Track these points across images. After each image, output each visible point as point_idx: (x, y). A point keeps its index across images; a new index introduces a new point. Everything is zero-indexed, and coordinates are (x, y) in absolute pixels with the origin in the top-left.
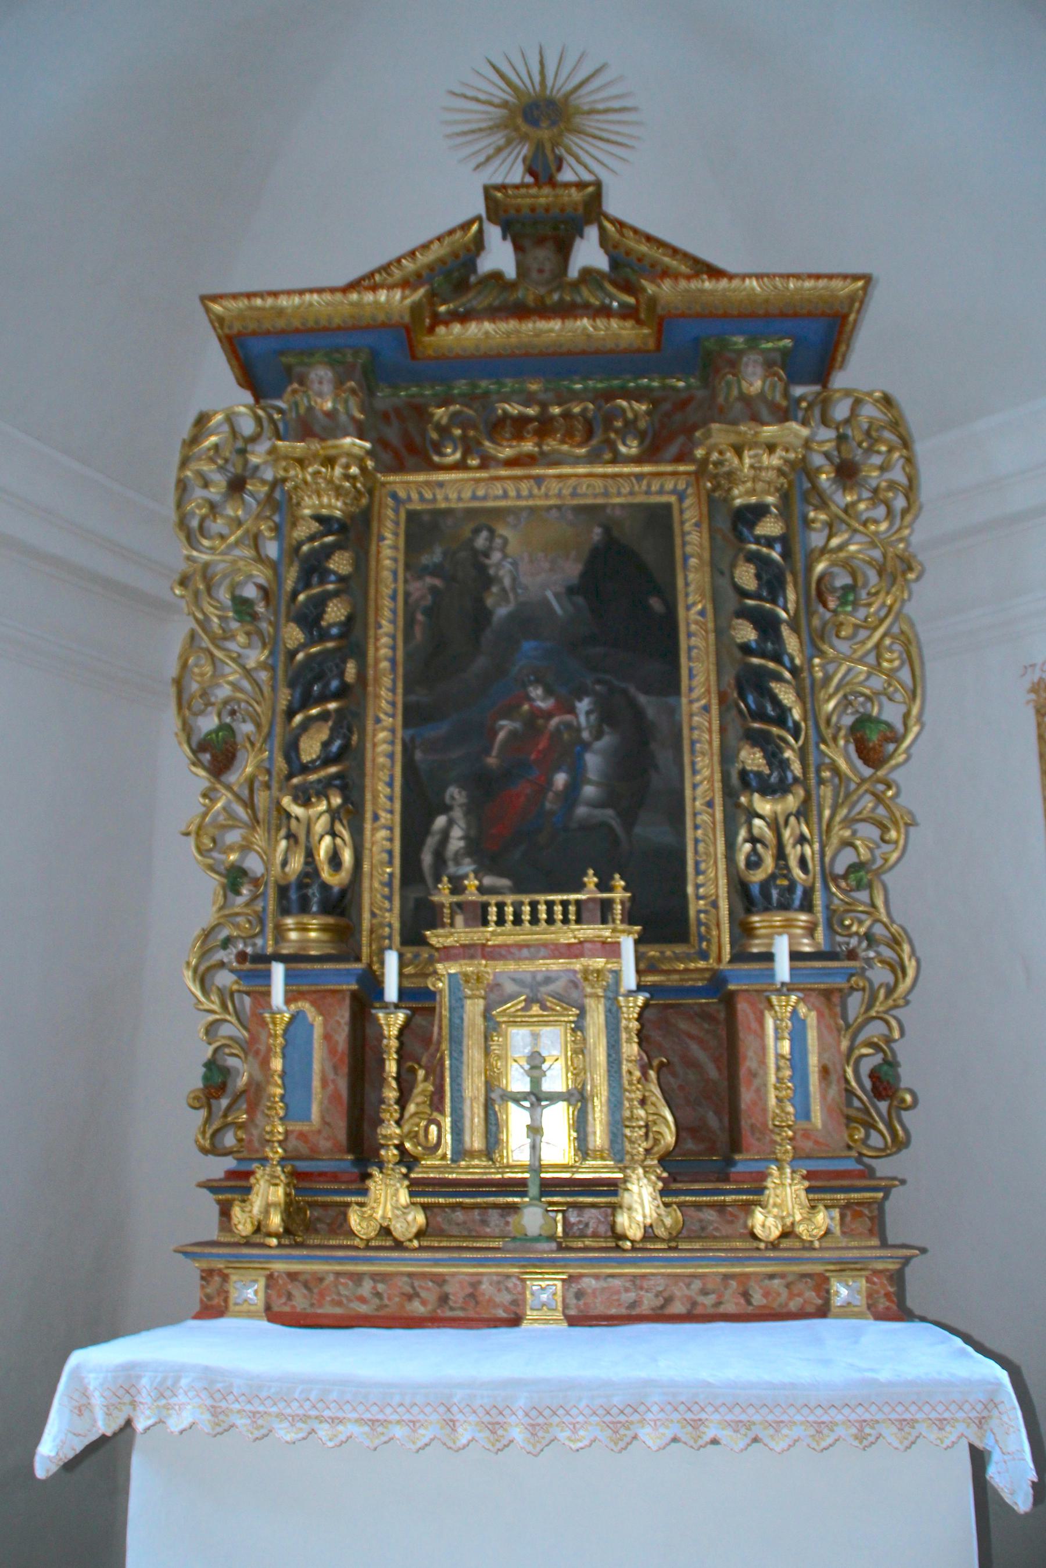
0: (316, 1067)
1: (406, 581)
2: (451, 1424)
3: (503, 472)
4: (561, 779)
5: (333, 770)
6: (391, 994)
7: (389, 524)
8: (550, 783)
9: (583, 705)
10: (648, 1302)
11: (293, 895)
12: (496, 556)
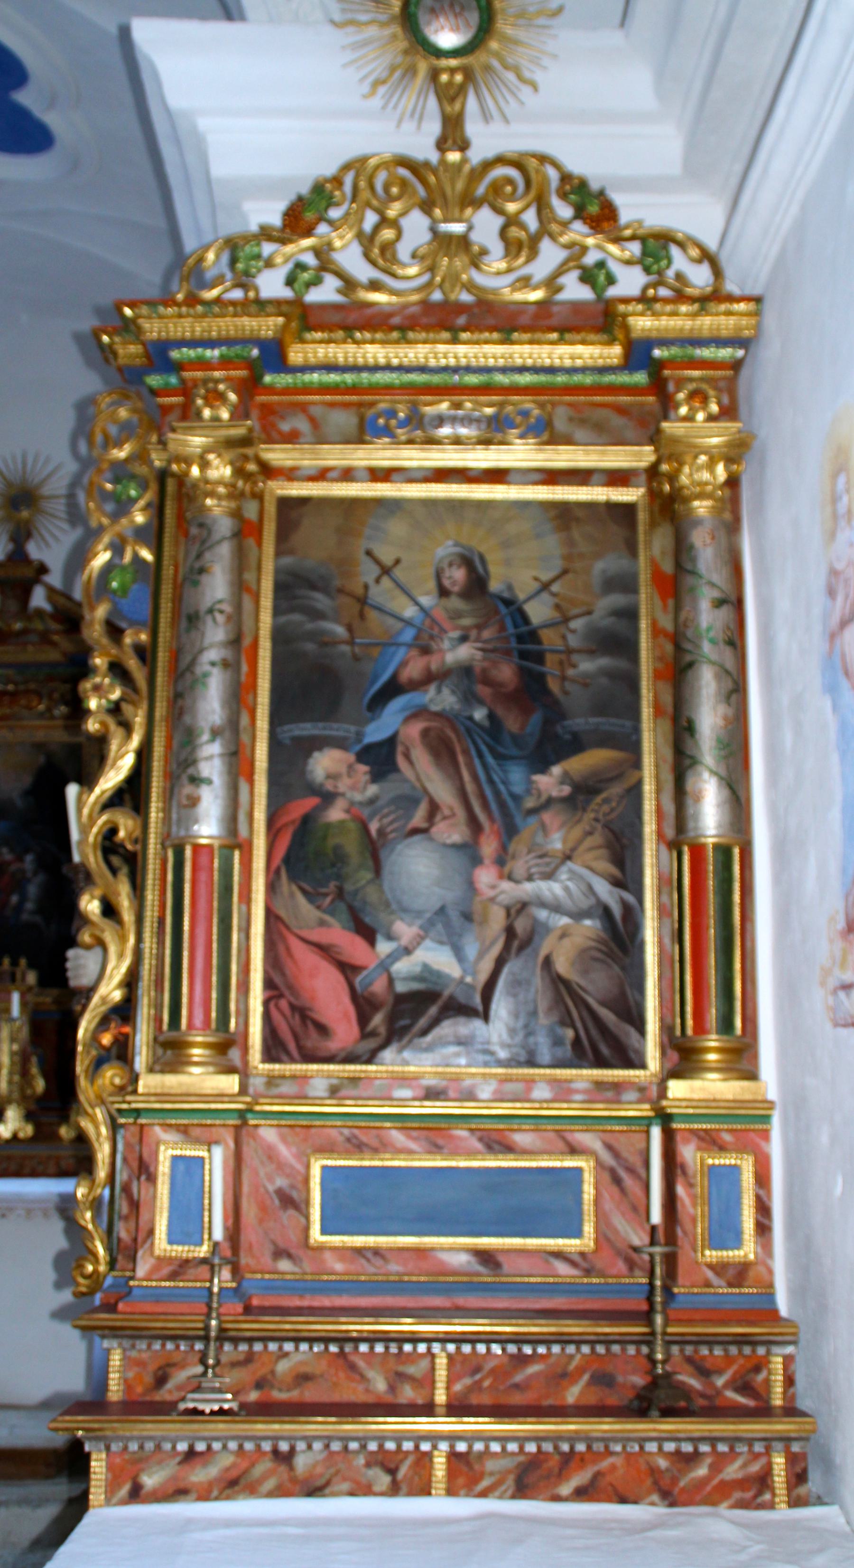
4: (14, 899)
9: (29, 858)
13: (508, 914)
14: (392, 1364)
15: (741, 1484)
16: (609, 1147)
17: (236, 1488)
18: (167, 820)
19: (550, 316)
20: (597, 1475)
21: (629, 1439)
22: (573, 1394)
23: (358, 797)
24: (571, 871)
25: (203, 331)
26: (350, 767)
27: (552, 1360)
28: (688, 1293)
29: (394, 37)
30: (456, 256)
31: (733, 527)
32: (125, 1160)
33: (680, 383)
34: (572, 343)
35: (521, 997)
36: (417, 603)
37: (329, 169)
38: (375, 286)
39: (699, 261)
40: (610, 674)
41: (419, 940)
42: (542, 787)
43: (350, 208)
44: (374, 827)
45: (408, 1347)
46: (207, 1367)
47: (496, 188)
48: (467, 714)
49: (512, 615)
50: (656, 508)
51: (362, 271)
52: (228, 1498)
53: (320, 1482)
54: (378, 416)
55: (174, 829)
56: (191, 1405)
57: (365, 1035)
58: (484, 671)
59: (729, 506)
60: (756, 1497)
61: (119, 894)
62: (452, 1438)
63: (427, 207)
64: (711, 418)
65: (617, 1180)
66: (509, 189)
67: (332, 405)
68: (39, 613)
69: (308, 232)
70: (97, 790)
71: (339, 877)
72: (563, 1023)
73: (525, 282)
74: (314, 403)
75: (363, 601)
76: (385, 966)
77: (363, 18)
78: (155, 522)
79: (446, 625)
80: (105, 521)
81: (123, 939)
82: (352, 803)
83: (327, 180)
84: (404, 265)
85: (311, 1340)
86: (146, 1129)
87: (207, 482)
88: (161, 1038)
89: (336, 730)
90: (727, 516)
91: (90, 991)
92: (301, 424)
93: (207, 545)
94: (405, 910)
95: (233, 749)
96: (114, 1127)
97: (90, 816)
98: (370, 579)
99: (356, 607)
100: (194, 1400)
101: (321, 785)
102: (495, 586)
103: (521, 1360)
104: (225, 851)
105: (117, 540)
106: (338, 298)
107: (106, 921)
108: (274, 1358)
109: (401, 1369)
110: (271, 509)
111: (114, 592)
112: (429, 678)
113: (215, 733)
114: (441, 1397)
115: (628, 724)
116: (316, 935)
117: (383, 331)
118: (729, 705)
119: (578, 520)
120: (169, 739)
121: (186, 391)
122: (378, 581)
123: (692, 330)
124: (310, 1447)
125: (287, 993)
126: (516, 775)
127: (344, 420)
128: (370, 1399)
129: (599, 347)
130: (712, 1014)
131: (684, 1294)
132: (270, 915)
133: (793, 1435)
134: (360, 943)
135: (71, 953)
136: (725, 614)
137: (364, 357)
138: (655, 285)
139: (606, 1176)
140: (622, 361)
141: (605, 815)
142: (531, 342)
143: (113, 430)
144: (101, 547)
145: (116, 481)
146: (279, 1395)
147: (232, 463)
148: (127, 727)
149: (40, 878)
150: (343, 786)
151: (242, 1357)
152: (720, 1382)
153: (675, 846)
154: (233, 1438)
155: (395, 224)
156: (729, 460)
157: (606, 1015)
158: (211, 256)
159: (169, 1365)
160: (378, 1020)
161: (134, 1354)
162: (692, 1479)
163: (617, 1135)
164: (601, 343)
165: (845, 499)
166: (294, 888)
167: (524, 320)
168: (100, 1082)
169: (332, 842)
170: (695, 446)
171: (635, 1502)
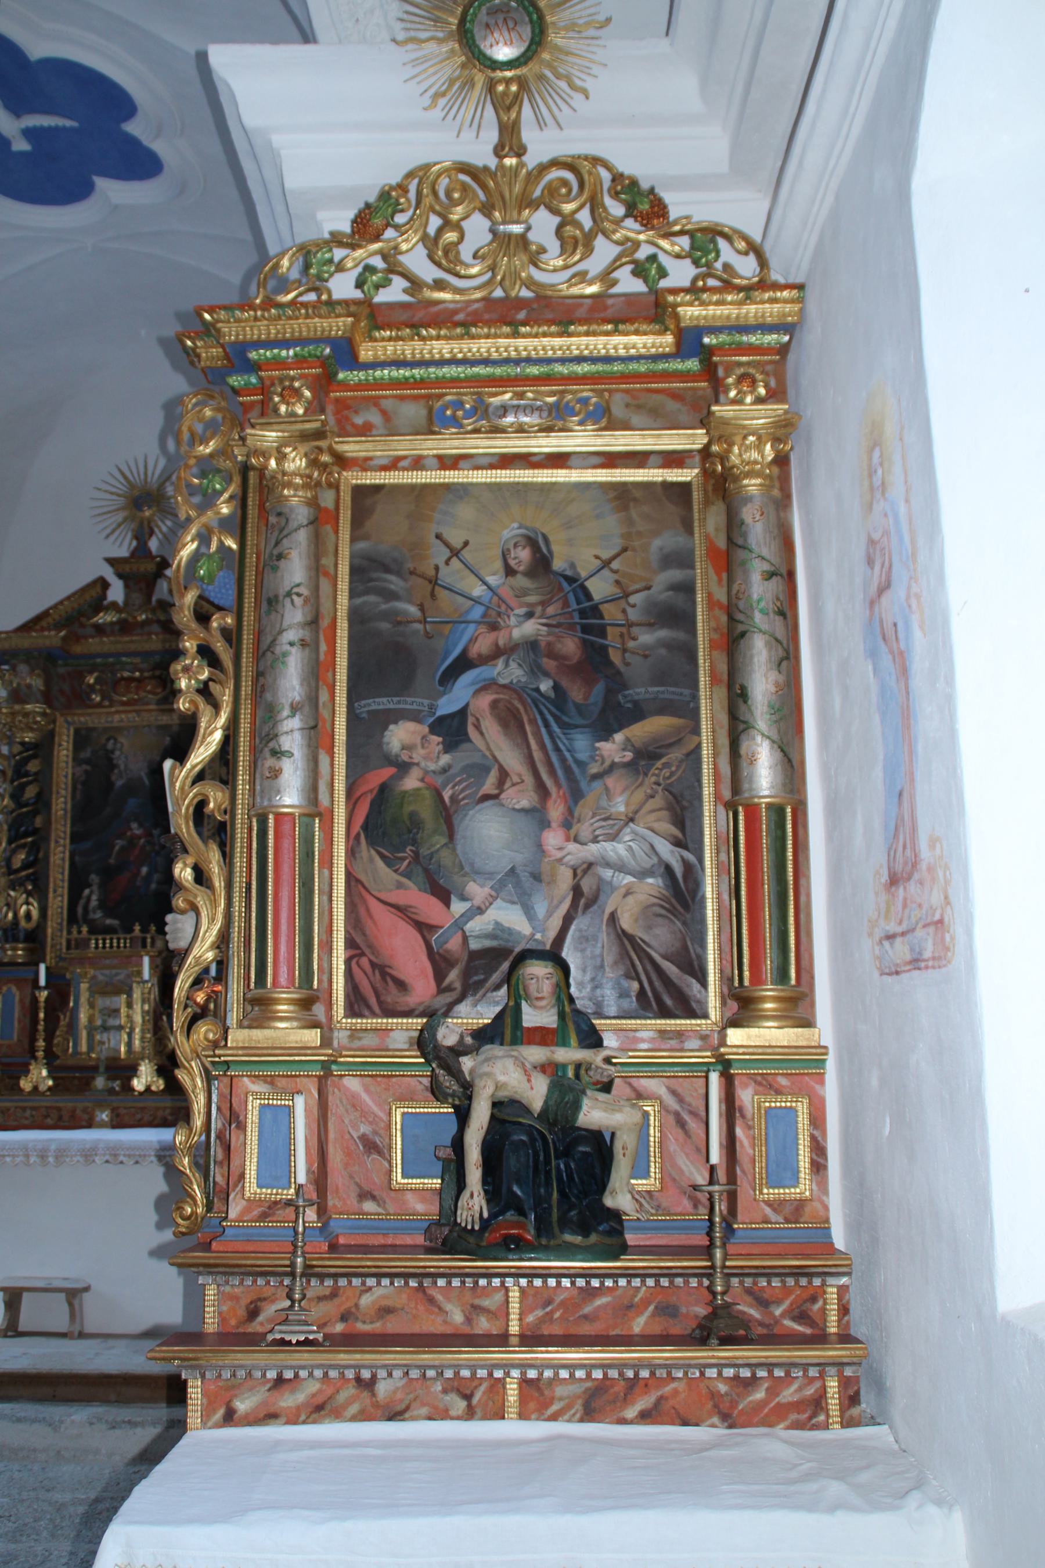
0: (16, 1015)
1: (73, 767)
2: (27, 1156)
3: (121, 708)
4: (144, 870)
5: (31, 871)
6: (42, 982)
7: (65, 738)
8: (139, 871)
11: (10, 933)
12: (117, 753)
13: (575, 875)
14: (468, 1296)
15: (796, 1406)
16: (673, 1092)
17: (322, 1413)
18: (252, 791)
19: (606, 308)
20: (660, 1400)
21: (690, 1366)
22: (639, 1325)
23: (432, 767)
24: (633, 832)
25: (278, 332)
26: (424, 737)
27: (619, 1292)
28: (747, 1228)
29: (452, 51)
30: (515, 256)
31: (783, 502)
32: (219, 1109)
33: (729, 368)
34: (626, 334)
35: (588, 952)
36: (485, 583)
37: (395, 179)
38: (440, 285)
39: (746, 254)
40: (668, 645)
41: (492, 900)
42: (605, 753)
43: (414, 214)
44: (447, 795)
45: (483, 1282)
46: (293, 1301)
47: (551, 190)
48: (533, 686)
49: (574, 591)
50: (710, 488)
51: (428, 272)
52: (314, 1422)
53: (401, 1407)
54: (446, 407)
55: (258, 799)
56: (278, 1336)
57: (441, 991)
58: (549, 644)
59: (777, 484)
60: (810, 1418)
61: (211, 862)
62: (524, 1366)
63: (486, 210)
64: (759, 400)
65: (681, 1123)
66: (564, 191)
67: (402, 398)
69: (377, 237)
70: (188, 766)
71: (414, 842)
72: (627, 976)
73: (582, 277)
74: (386, 397)
75: (434, 582)
76: (459, 925)
77: (424, 35)
78: (239, 512)
79: (513, 602)
80: (193, 513)
81: (214, 903)
82: (426, 772)
83: (392, 188)
84: (467, 266)
85: (392, 1276)
86: (235, 1080)
87: (284, 474)
88: (249, 996)
89: (409, 703)
90: (776, 492)
91: (187, 951)
92: (374, 417)
93: (285, 533)
94: (478, 873)
95: (312, 724)
96: (209, 1078)
97: (182, 788)
98: (440, 561)
99: (429, 587)
100: (281, 1332)
101: (397, 756)
102: (558, 565)
103: (590, 1293)
104: (305, 819)
105: (203, 530)
106: (407, 298)
107: (198, 887)
108: (358, 1293)
109: (477, 1302)
110: (346, 498)
111: (202, 579)
112: (497, 653)
113: (295, 709)
114: (514, 1328)
115: (687, 692)
116: (393, 898)
117: (448, 328)
118: (780, 672)
119: (635, 500)
120: (254, 715)
121: (264, 389)
122: (447, 563)
123: (738, 317)
124: (390, 1375)
125: (367, 951)
126: (581, 742)
127: (412, 412)
128: (449, 1330)
129: (652, 337)
130: (769, 965)
131: (743, 1228)
132: (349, 875)
133: (845, 1360)
134: (435, 903)
135: (169, 918)
136: (775, 586)
137: (430, 352)
138: (704, 277)
139: (671, 1119)
140: (674, 350)
141: (665, 778)
142: (587, 334)
143: (199, 428)
144: (189, 538)
145: (203, 475)
146: (362, 1327)
147: (306, 455)
148: (216, 707)
151: (327, 1292)
152: (778, 1312)
153: (731, 806)
154: (319, 1366)
155: (457, 227)
156: (776, 440)
157: (671, 969)
158: (285, 262)
159: (260, 1299)
160: (453, 976)
161: (228, 1289)
162: (750, 1402)
163: (681, 1080)
164: (654, 334)
165: (880, 472)
166: (373, 852)
167: (581, 313)
168: (194, 1037)
169: (408, 809)
170: (744, 427)
171: (697, 1425)
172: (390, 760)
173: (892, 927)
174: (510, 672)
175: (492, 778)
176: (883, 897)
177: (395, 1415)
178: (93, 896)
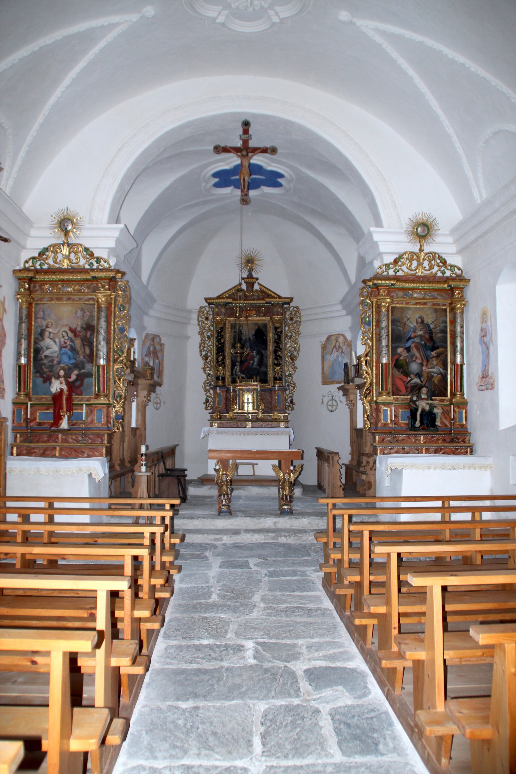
4: (251, 362)
9: (255, 352)
10: (260, 426)
68: (257, 291)
75: (405, 324)
102: (425, 322)
112: (415, 337)
126: (429, 352)
132: (392, 374)
149: (258, 357)
150: (403, 353)
172: (398, 354)
173: (482, 384)
174: (417, 340)
175: (414, 358)
176: (480, 380)
177: (408, 453)
178: (237, 368)
